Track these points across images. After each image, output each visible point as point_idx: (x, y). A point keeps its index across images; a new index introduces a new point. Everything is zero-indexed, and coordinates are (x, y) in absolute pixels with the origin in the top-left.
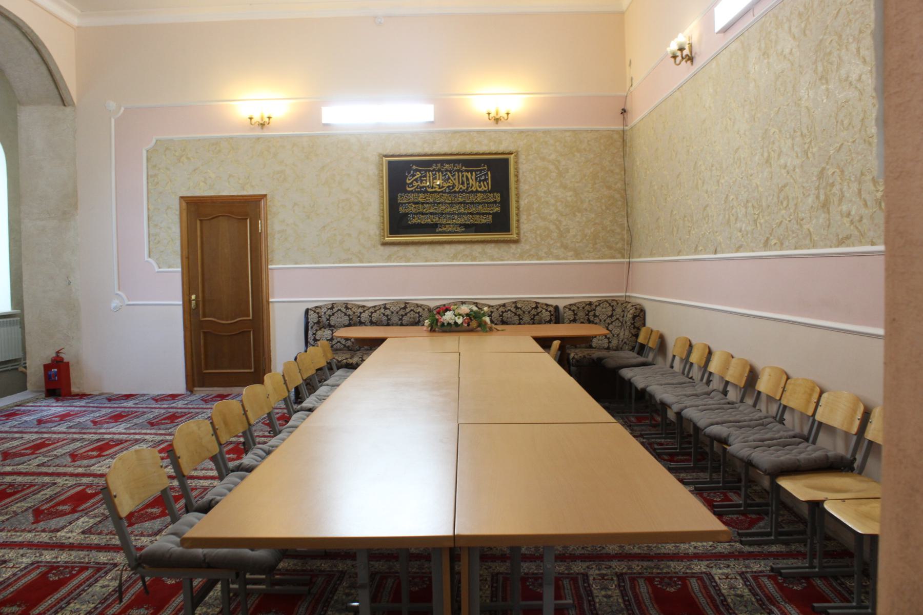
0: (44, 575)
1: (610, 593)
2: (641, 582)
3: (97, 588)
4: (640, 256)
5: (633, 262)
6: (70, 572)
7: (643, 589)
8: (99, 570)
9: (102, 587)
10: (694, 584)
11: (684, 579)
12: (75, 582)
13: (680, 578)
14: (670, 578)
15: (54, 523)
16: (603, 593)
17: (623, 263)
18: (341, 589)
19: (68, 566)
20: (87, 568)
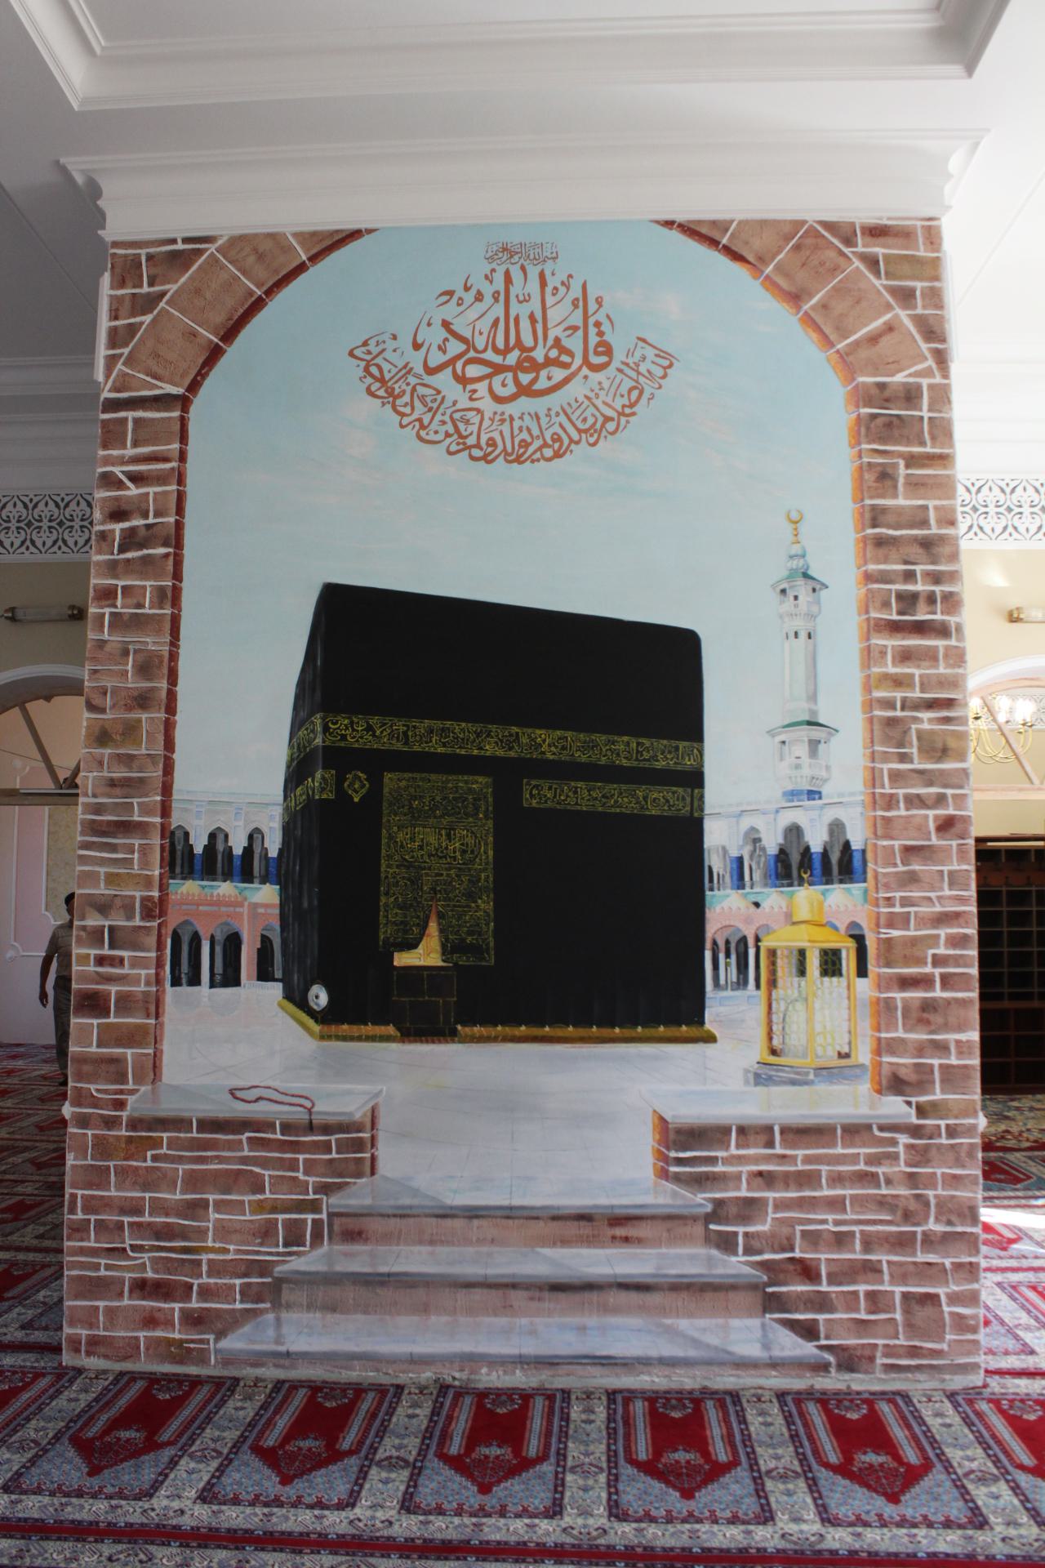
0: (146, 1394)
1: (769, 1420)
2: (710, 1404)
3: (61, 1402)
4: (211, 341)
5: (216, 335)
6: (22, 1380)
7: (639, 1408)
8: (59, 1377)
9: (70, 1400)
10: (885, 1408)
11: (870, 1400)
12: (25, 1396)
13: (865, 1401)
14: (852, 1401)
15: (128, 1475)
16: (760, 1419)
17: (170, 418)
18: (400, 1410)
19: (33, 1264)
20: (44, 1375)
